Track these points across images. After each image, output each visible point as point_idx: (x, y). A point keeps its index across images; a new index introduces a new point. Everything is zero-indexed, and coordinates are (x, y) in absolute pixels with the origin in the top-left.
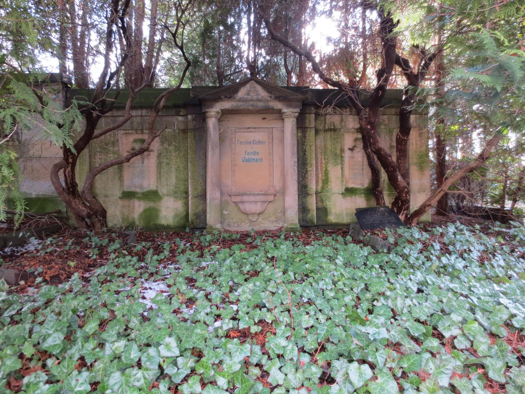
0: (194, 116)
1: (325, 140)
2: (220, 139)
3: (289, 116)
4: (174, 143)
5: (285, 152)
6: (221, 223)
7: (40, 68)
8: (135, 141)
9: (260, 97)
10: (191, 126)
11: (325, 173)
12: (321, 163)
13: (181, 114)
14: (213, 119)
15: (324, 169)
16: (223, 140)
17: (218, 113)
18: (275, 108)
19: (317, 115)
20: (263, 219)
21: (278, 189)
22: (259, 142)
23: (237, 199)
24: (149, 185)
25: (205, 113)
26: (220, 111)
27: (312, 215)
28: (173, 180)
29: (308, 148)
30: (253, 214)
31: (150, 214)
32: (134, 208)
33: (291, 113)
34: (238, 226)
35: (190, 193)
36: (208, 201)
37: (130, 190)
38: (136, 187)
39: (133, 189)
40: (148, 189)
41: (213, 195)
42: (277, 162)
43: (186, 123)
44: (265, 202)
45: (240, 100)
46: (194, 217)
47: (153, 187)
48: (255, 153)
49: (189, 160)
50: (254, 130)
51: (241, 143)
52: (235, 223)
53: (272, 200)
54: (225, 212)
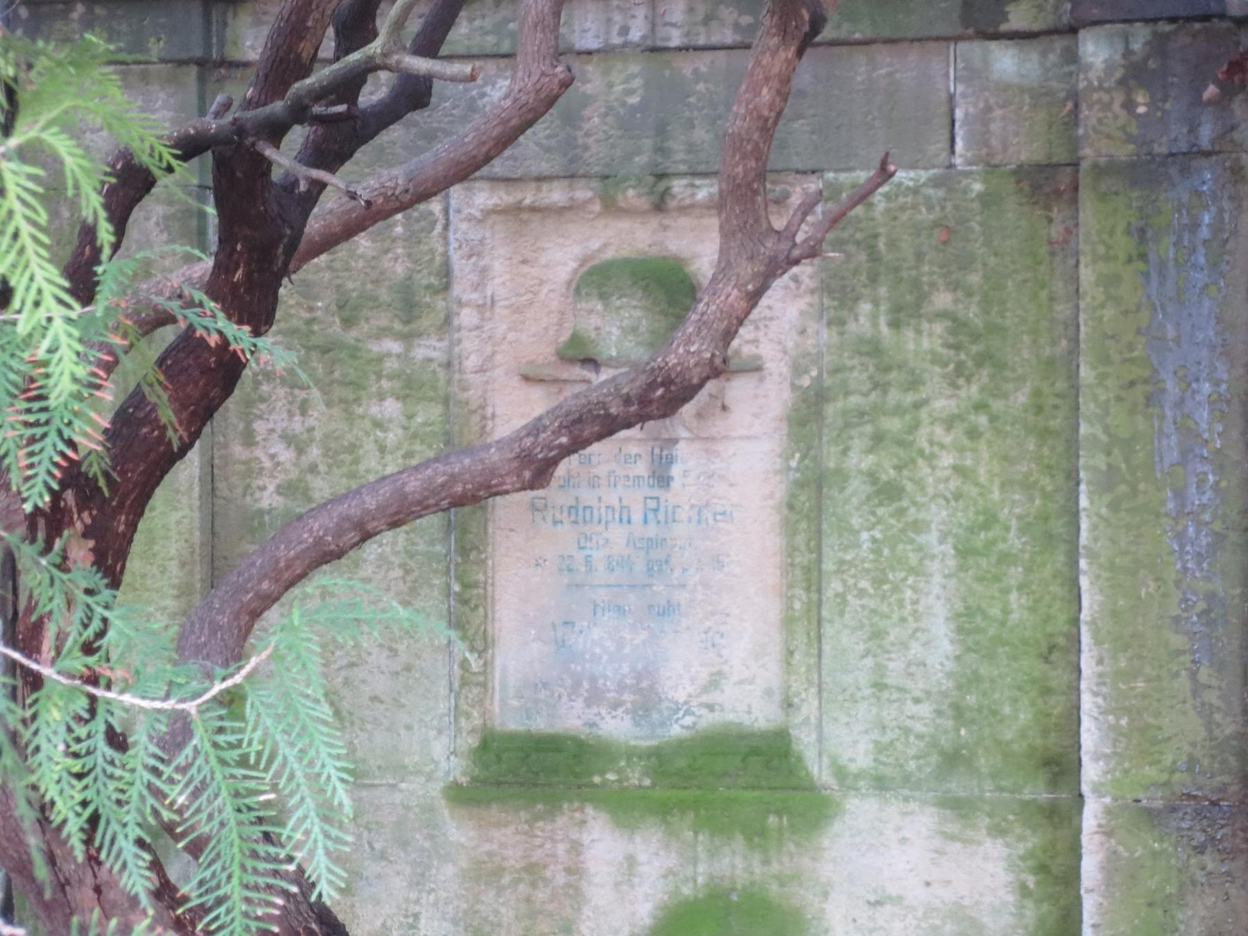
0: (1140, 37)
4: (942, 300)
8: (597, 279)
10: (1106, 134)
24: (714, 682)
28: (933, 647)
32: (574, 893)
35: (1091, 772)
37: (540, 725)
38: (595, 697)
39: (571, 719)
40: (707, 720)
47: (747, 704)
49: (1090, 462)
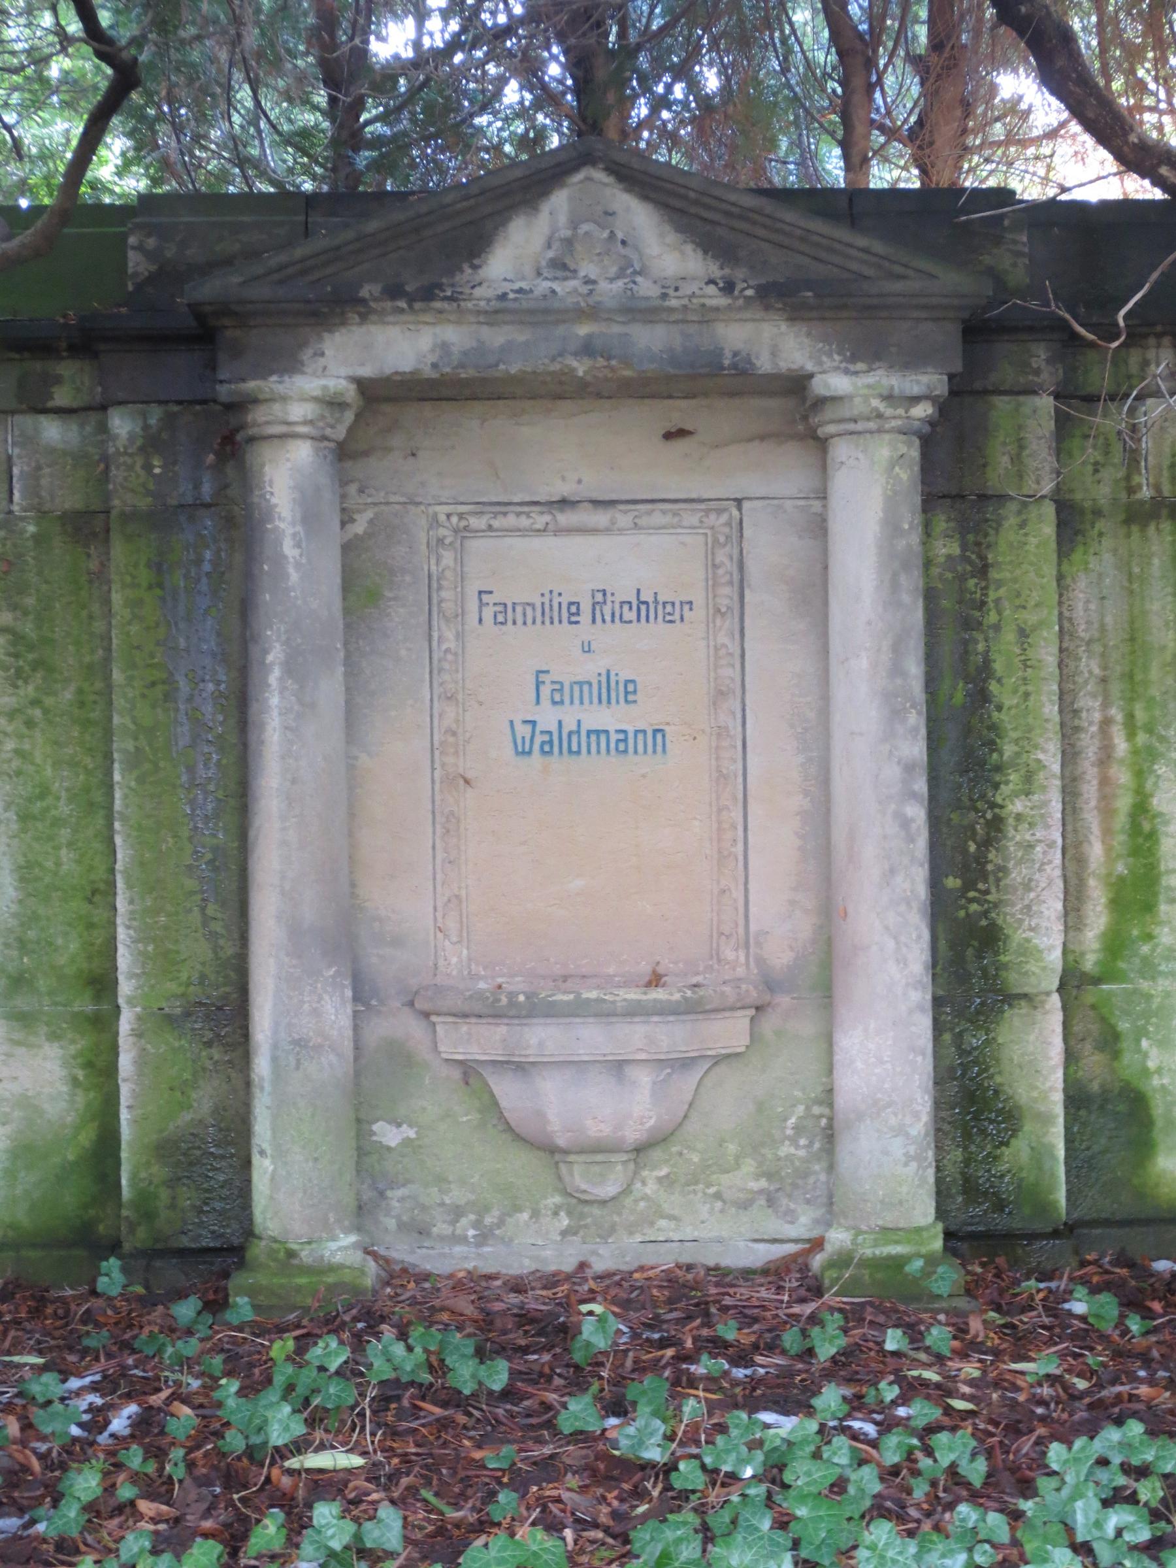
0: (155, 414)
1: (1133, 585)
2: (348, 586)
3: (867, 426)
5: (839, 692)
6: (362, 1214)
9: (646, 288)
10: (130, 489)
11: (1135, 828)
12: (1106, 756)
13: (62, 397)
14: (302, 453)
15: (1124, 803)
16: (374, 597)
17: (334, 403)
18: (764, 364)
19: (1075, 400)
20: (667, 1182)
21: (780, 957)
22: (643, 608)
23: (480, 1042)
25: (240, 406)
26: (350, 392)
27: (1040, 1153)
29: (1004, 650)
30: (598, 1150)
33: (877, 402)
34: (484, 1237)
35: (126, 987)
36: (262, 1066)
41: (293, 1010)
42: (774, 758)
43: (98, 465)
44: (685, 1063)
45: (502, 310)
46: (159, 1172)
49: (122, 746)
50: (601, 518)
51: (505, 614)
52: (457, 1212)
53: (740, 1042)
54: (389, 1135)
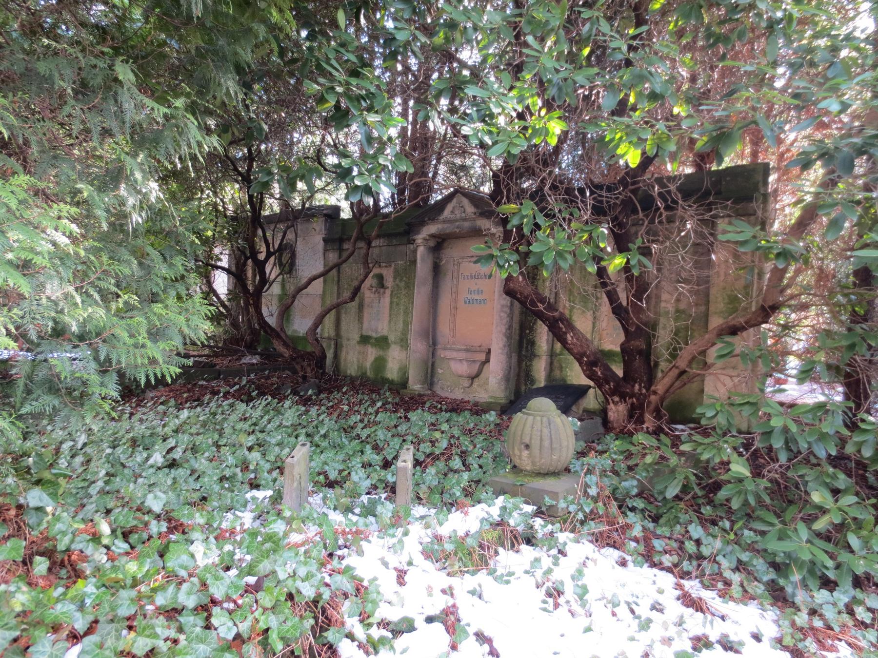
7: (407, 155)
31: (380, 363)
45: (445, 221)
48: (480, 292)
51: (465, 278)
